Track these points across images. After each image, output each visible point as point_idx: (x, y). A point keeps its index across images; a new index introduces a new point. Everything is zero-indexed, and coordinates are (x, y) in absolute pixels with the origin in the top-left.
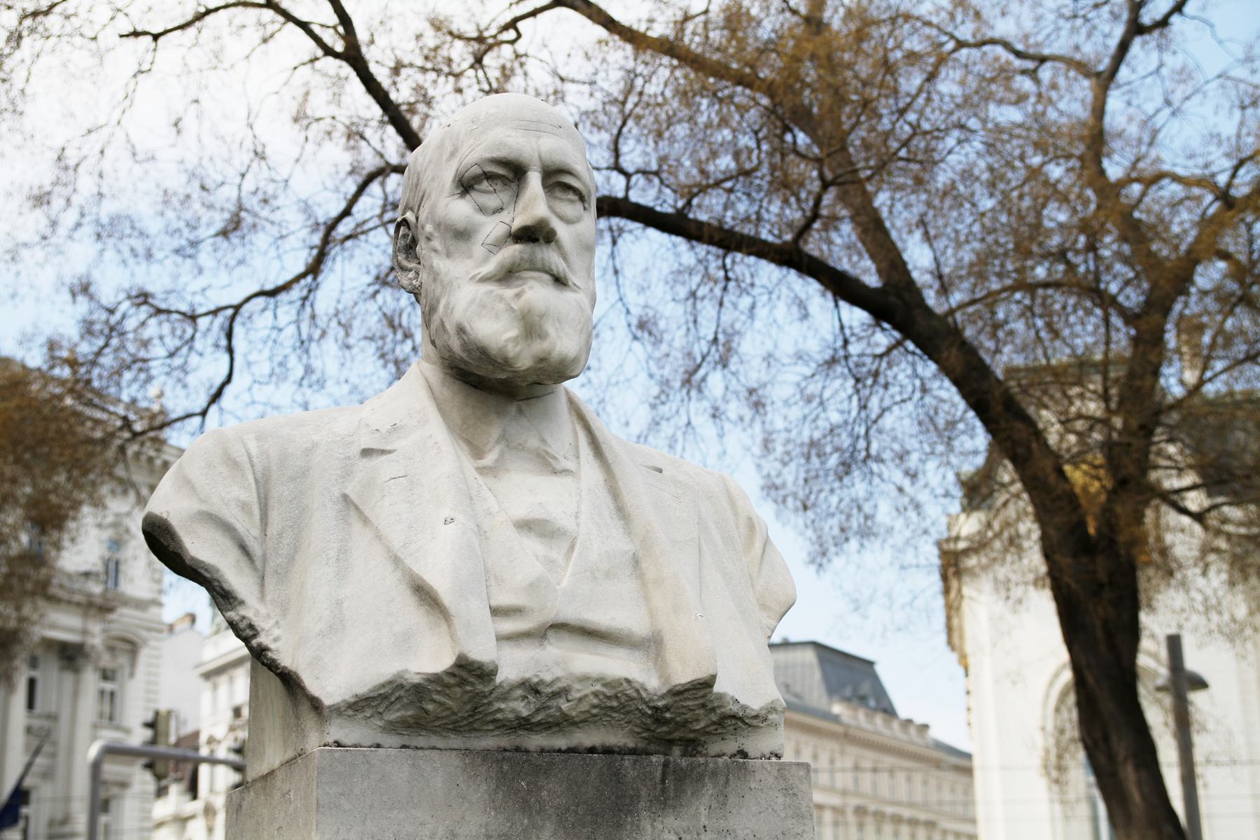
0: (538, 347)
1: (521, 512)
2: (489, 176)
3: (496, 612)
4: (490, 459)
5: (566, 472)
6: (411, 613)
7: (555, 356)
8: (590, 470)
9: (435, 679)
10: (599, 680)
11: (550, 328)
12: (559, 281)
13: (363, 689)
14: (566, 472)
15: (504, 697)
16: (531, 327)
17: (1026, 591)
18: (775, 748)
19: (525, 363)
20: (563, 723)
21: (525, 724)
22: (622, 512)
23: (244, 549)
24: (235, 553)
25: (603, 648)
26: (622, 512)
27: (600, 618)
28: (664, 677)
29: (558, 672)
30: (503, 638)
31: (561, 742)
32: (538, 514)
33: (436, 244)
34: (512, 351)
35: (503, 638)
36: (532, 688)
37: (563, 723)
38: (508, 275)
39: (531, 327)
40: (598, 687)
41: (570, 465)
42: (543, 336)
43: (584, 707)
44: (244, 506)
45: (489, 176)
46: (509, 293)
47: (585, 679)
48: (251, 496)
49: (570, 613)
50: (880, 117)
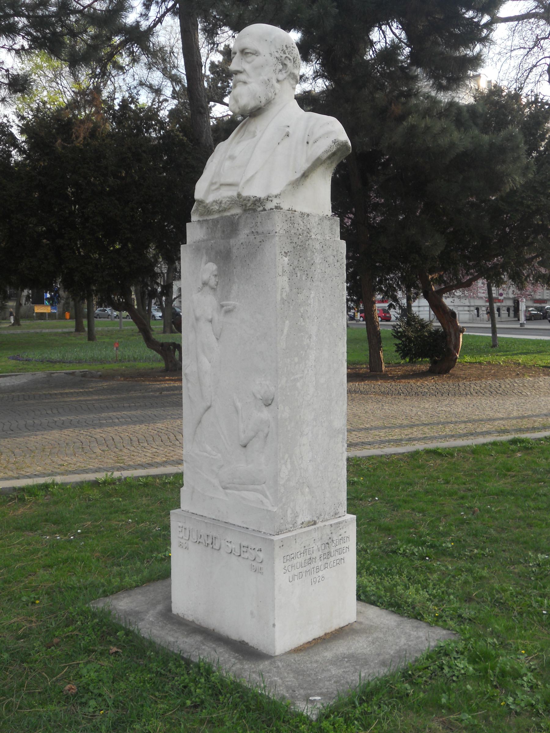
12: (245, 83)
15: (212, 205)
18: (271, 407)
29: (219, 197)
37: (225, 210)
40: (228, 199)
43: (227, 204)
47: (224, 198)
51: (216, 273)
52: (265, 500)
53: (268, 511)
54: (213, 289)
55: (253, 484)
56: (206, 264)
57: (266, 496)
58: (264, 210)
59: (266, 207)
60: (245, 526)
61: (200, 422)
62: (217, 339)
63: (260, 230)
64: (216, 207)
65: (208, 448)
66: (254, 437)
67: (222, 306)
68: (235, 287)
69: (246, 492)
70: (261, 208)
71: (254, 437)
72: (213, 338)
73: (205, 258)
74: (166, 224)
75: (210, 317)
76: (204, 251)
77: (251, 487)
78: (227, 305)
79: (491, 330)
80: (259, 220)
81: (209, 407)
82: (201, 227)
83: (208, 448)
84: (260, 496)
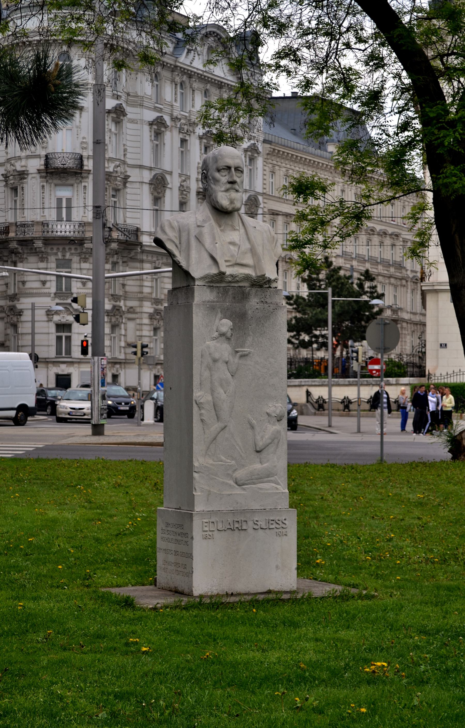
0: (233, 206)
1: (228, 240)
2: (223, 169)
3: (226, 261)
4: (222, 228)
5: (237, 230)
6: (209, 261)
7: (236, 208)
8: (242, 230)
9: (215, 274)
10: (244, 274)
11: (235, 202)
13: (202, 276)
14: (237, 230)
16: (232, 202)
17: (299, 351)
18: (281, 422)
19: (230, 209)
20: (238, 282)
21: (230, 282)
22: (248, 239)
23: (177, 246)
24: (175, 247)
25: (244, 268)
26: (248, 239)
27: (244, 262)
28: (256, 273)
30: (227, 266)
31: (236, 285)
32: (232, 241)
33: (212, 181)
34: (228, 207)
35: (227, 266)
36: (232, 276)
37: (238, 282)
38: (227, 190)
39: (232, 202)
41: (238, 228)
42: (234, 203)
44: (176, 237)
45: (223, 169)
46: (227, 194)
47: (241, 274)
48: (177, 235)
49: (238, 261)
50: (254, 657)
51: (232, 327)
52: (278, 487)
53: (283, 493)
54: (228, 339)
55: (268, 476)
56: (221, 320)
57: (278, 484)
58: (270, 287)
59: (271, 286)
60: (263, 508)
61: (215, 439)
62: (232, 376)
63: (269, 301)
64: (230, 279)
65: (223, 458)
66: (270, 443)
67: (237, 352)
68: (250, 339)
69: (261, 484)
70: (267, 286)
71: (270, 443)
72: (229, 375)
73: (219, 315)
74: (339, 334)
75: (227, 359)
76: (219, 310)
77: (266, 479)
78: (242, 351)
79: (91, 295)
80: (268, 293)
81: (225, 427)
82: (211, 291)
83: (223, 458)
84: (274, 485)
